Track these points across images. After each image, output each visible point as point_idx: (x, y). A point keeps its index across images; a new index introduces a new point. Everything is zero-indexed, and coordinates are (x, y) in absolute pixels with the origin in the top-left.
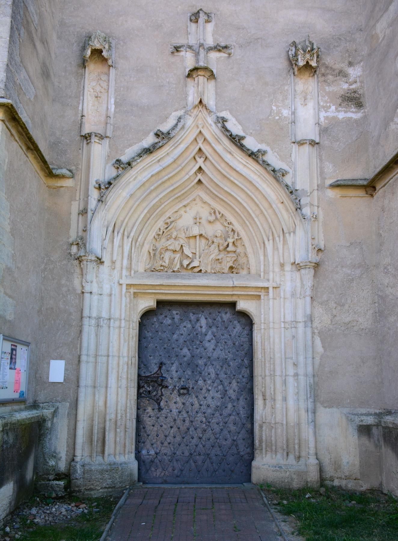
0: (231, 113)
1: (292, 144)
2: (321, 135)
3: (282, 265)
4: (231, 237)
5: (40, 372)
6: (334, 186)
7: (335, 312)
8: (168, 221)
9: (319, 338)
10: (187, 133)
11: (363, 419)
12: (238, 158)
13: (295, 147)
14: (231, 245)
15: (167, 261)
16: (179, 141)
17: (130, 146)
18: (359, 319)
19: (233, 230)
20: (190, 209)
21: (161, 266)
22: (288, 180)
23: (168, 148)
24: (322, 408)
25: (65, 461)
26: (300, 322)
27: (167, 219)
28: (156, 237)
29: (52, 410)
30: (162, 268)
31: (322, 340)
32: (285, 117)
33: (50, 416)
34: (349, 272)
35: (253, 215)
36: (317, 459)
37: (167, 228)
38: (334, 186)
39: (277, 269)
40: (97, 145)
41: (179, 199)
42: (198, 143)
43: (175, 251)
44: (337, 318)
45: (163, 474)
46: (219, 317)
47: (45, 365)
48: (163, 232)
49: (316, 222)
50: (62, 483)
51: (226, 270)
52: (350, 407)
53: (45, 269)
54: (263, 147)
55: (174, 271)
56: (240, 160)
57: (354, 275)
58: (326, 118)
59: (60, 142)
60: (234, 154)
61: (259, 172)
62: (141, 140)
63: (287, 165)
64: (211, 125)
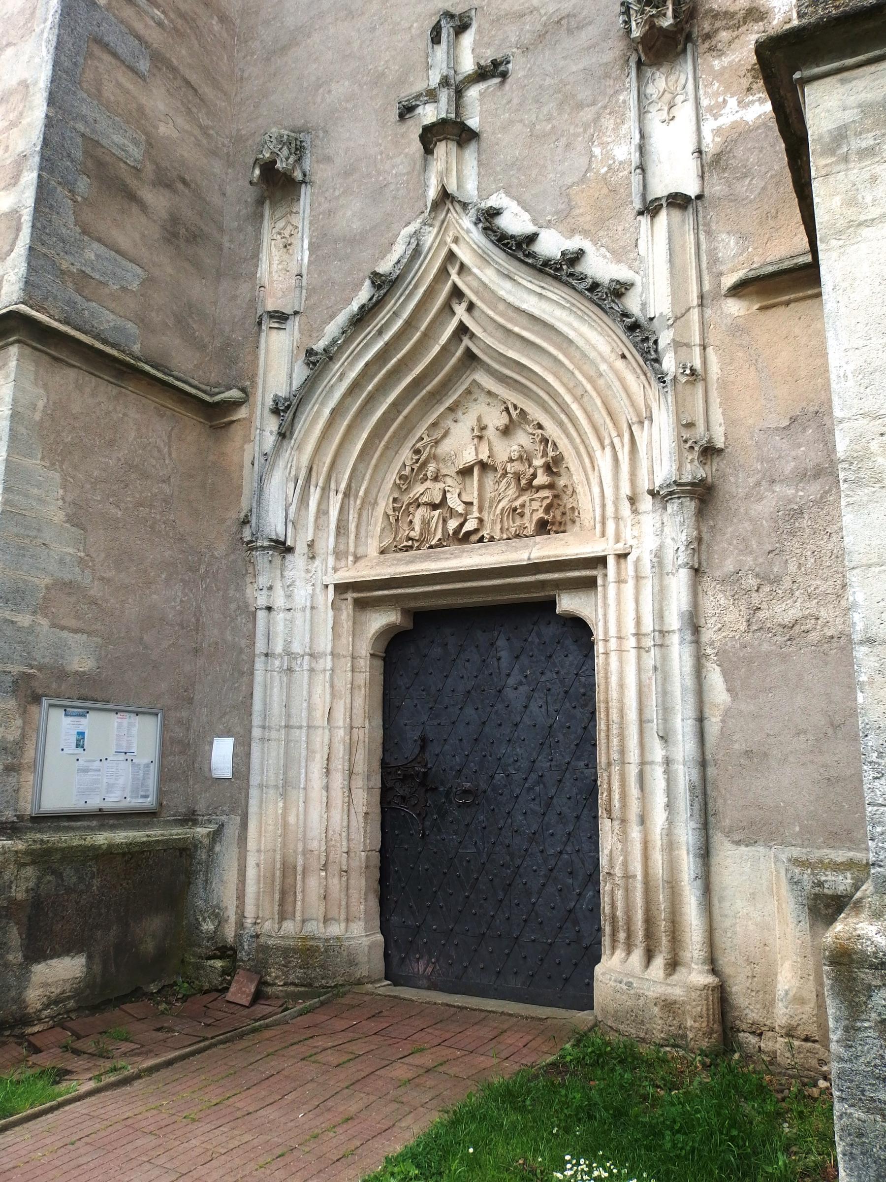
0: (508, 194)
1: (639, 218)
2: (707, 175)
5: (199, 759)
6: (739, 289)
7: (756, 599)
8: (419, 445)
9: (718, 669)
10: (427, 261)
11: (823, 878)
12: (524, 283)
14: (540, 472)
15: (417, 528)
16: (413, 283)
17: (332, 317)
18: (822, 609)
20: (464, 413)
22: (632, 303)
23: (393, 302)
24: (728, 845)
25: (234, 925)
26: (673, 631)
27: (417, 442)
28: (398, 482)
29: (213, 827)
31: (725, 673)
32: (620, 163)
33: (206, 841)
34: (791, 492)
35: (568, 399)
36: (714, 971)
38: (739, 289)
40: (274, 333)
41: (437, 396)
42: (449, 275)
44: (761, 615)
45: (429, 970)
46: (533, 634)
47: (207, 748)
48: (413, 469)
49: (700, 387)
50: (219, 964)
51: (531, 528)
52: (802, 846)
53: (207, 572)
54: (573, 244)
55: (431, 547)
56: (529, 285)
57: (801, 497)
58: (717, 132)
59: (228, 345)
60: (516, 277)
61: (568, 302)
62: (349, 301)
63: (630, 268)
64: (468, 232)
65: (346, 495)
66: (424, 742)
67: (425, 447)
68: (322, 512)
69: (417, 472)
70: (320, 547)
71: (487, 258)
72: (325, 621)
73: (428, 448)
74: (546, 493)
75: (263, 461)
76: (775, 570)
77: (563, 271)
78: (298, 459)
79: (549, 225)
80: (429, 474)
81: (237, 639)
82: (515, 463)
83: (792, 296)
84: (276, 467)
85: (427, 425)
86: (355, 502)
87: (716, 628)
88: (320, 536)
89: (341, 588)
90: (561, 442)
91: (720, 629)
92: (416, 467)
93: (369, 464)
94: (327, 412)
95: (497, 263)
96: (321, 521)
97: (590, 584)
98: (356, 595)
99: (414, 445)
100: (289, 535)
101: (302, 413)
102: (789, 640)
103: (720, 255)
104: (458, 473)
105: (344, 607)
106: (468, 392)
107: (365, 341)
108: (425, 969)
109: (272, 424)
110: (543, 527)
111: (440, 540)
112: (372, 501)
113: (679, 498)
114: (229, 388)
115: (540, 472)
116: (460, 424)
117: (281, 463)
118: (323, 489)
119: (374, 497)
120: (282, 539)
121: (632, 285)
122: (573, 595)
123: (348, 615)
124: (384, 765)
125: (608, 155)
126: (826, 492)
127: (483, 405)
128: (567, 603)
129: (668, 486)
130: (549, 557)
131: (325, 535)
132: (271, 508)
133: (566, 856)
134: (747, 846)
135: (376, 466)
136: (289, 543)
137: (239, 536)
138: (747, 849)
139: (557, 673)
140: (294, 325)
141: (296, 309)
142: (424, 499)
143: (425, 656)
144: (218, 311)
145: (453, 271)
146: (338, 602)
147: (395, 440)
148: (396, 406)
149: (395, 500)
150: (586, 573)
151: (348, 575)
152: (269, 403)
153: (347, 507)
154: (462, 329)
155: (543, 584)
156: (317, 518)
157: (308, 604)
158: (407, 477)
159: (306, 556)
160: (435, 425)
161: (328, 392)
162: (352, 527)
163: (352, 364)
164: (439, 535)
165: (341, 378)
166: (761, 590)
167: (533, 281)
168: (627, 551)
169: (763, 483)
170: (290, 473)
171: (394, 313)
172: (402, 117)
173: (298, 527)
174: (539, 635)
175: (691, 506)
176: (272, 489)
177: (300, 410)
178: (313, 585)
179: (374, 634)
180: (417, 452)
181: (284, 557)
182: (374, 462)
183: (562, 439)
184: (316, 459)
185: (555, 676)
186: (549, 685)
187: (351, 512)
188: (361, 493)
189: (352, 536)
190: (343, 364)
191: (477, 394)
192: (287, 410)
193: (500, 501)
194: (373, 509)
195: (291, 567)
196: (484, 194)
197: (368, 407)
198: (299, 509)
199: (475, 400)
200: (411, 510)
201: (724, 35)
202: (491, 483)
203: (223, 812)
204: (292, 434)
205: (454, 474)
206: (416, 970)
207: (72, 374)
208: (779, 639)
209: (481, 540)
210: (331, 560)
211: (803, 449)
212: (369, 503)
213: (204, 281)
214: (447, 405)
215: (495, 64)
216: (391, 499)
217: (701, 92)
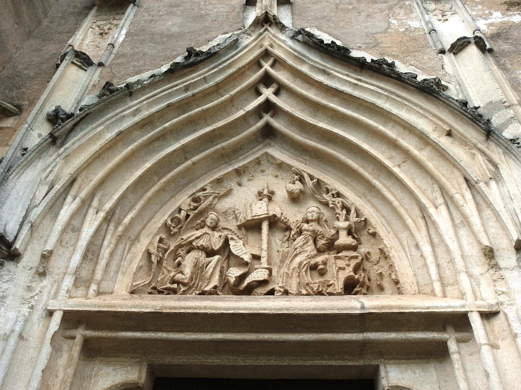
3: (489, 253)
4: (342, 218)
13: (447, 58)
16: (228, 62)
19: (344, 207)
20: (249, 180)
21: (173, 282)
23: (206, 69)
27: (198, 191)
30: (175, 286)
37: (196, 208)
39: (479, 267)
40: (74, 68)
43: (210, 253)
48: (188, 216)
51: (339, 286)
55: (203, 293)
61: (386, 90)
65: (107, 220)
67: (206, 197)
68: (72, 227)
69: (197, 216)
70: (57, 264)
72: (34, 362)
73: (211, 198)
75: (19, 154)
78: (62, 169)
80: (208, 222)
84: (32, 167)
85: (211, 179)
86: (116, 227)
88: (60, 253)
89: (72, 319)
90: (366, 210)
92: (192, 215)
93: (141, 197)
94: (110, 135)
95: (312, 61)
96: (67, 237)
97: (438, 353)
98: (90, 333)
99: (194, 194)
100: (22, 237)
101: (82, 130)
104: (240, 227)
105: (66, 347)
106: (258, 162)
107: (170, 91)
109: (44, 130)
110: (350, 287)
111: (215, 287)
112: (133, 237)
115: (343, 234)
116: (243, 189)
117: (40, 165)
118: (83, 202)
119: (136, 233)
120: (10, 238)
122: (414, 367)
123: (70, 358)
127: (271, 177)
130: (391, 307)
131: (67, 254)
132: (8, 202)
135: (150, 199)
136: (18, 245)
141: (103, 61)
142: (201, 242)
144: (17, 55)
146: (59, 339)
147: (173, 185)
148: (185, 152)
149: (161, 241)
151: (88, 302)
152: (50, 108)
153: (103, 232)
155: (363, 347)
156: (64, 231)
157: (18, 329)
158: (179, 220)
159: (33, 271)
160: (219, 181)
161: (117, 120)
162: (105, 253)
163: (150, 105)
164: (215, 281)
165: (135, 113)
167: (350, 74)
168: (494, 309)
170: (47, 177)
171: (204, 77)
173: (35, 235)
176: (18, 186)
177: (81, 125)
178: (32, 308)
180: (196, 200)
182: (149, 194)
183: (366, 208)
184: (84, 173)
187: (108, 237)
188: (126, 220)
189: (102, 263)
190: (141, 102)
191: (265, 165)
192: (63, 126)
193: (296, 255)
194: (131, 245)
195: (6, 278)
197: (157, 144)
198: (43, 216)
199: (263, 171)
200: (181, 252)
202: (279, 242)
204: (63, 144)
209: (272, 292)
210: (68, 282)
212: (129, 237)
213: (16, 26)
214: (236, 166)
216: (158, 238)
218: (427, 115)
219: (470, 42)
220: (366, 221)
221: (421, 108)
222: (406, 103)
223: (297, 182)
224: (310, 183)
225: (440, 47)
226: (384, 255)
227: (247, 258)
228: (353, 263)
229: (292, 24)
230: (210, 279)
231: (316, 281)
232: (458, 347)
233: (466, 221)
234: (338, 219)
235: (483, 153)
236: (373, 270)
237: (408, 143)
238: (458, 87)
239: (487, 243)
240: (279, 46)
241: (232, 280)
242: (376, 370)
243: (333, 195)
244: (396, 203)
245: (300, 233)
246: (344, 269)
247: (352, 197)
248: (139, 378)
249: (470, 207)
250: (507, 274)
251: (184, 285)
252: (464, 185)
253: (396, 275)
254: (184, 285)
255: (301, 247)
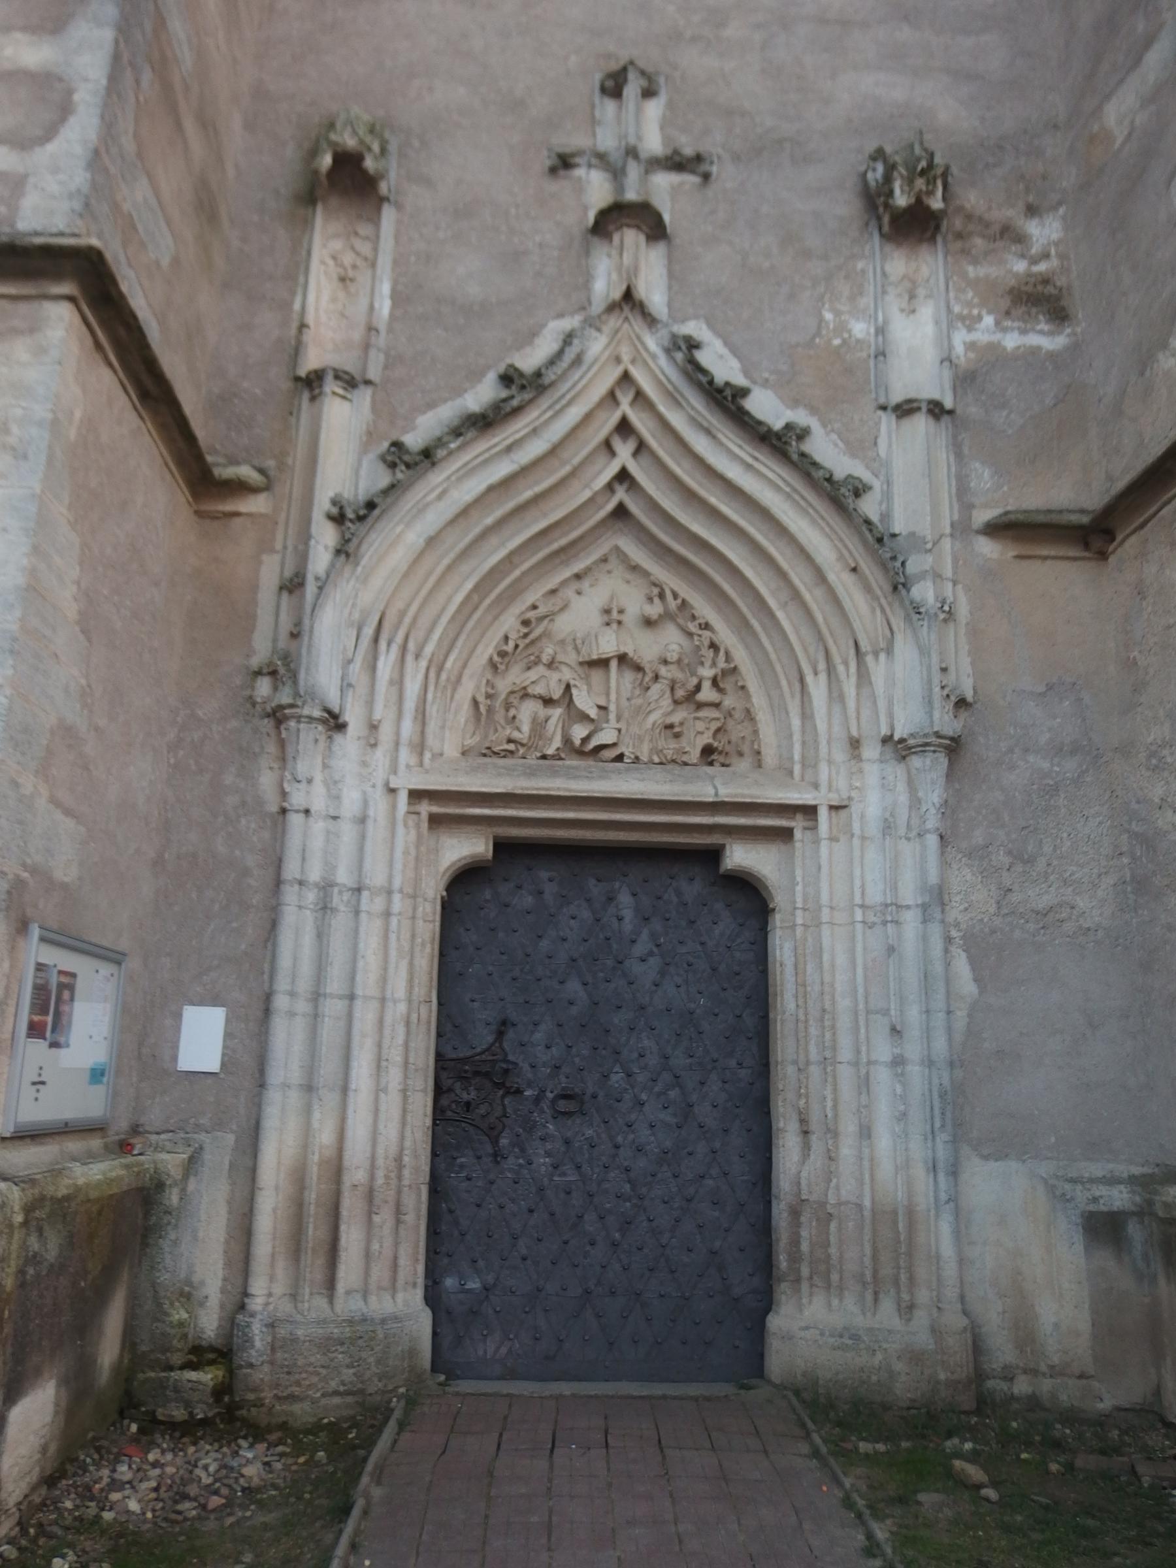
1: (880, 413)
3: (855, 744)
4: (708, 663)
6: (999, 529)
7: (1007, 880)
8: (531, 615)
9: (964, 955)
11: (1098, 1194)
13: (887, 421)
14: (707, 685)
15: (526, 728)
16: (568, 397)
17: (431, 406)
19: (713, 646)
20: (592, 586)
21: (510, 741)
22: (869, 507)
24: (976, 1161)
30: (511, 747)
31: (972, 961)
32: (858, 341)
34: (1046, 765)
37: (526, 635)
38: (999, 529)
40: (338, 400)
43: (548, 702)
44: (1015, 898)
45: (504, 1350)
47: (168, 1022)
48: (517, 646)
51: (695, 755)
55: (544, 757)
56: (737, 450)
57: (1058, 773)
60: (720, 436)
61: (788, 484)
62: (458, 392)
63: (867, 467)
66: (503, 1027)
71: (678, 397)
74: (714, 713)
76: (1030, 848)
77: (778, 443)
79: (765, 384)
80: (545, 658)
81: (237, 853)
82: (672, 667)
83: (1053, 553)
87: (962, 907)
89: (416, 795)
91: (966, 909)
92: (521, 646)
95: (693, 408)
97: (786, 835)
98: (436, 809)
99: (523, 613)
102: (1043, 928)
103: (972, 484)
106: (604, 560)
108: (498, 1348)
111: (558, 749)
113: (934, 752)
114: (237, 463)
115: (707, 685)
121: (870, 488)
122: (749, 846)
124: (439, 1057)
125: (841, 328)
126: (1083, 772)
128: (739, 856)
129: (925, 735)
130: (743, 796)
133: (710, 1182)
134: (996, 1160)
137: (248, 693)
138: (998, 1163)
139: (702, 944)
140: (364, 396)
143: (507, 906)
145: (625, 400)
150: (780, 824)
154: (623, 476)
160: (553, 592)
166: (1012, 870)
169: (1017, 750)
172: (553, 170)
174: (679, 893)
175: (943, 760)
179: (448, 869)
180: (526, 623)
181: (330, 737)
185: (699, 948)
186: (691, 959)
191: (614, 562)
192: (355, 519)
196: (677, 315)
199: (609, 572)
200: (514, 700)
201: (978, 242)
203: (198, 1128)
205: (573, 664)
206: (481, 1353)
207: (106, 375)
208: (1031, 926)
209: (620, 758)
211: (1059, 720)
215: (699, 158)
217: (952, 295)
218: (834, 537)
219: (919, 409)
220: (735, 668)
221: (828, 524)
222: (811, 511)
223: (656, 600)
224: (673, 604)
225: (882, 400)
226: (749, 716)
227: (593, 713)
228: (714, 726)
229: (670, 305)
230: (551, 740)
231: (670, 747)
232: (803, 834)
233: (842, 698)
234: (702, 663)
235: (883, 611)
236: (737, 731)
237: (799, 577)
238: (885, 487)
239: (855, 733)
240: (645, 363)
241: (577, 742)
242: (723, 846)
243: (700, 625)
244: (773, 656)
245: (656, 677)
246: (702, 733)
247: (725, 634)
248: (487, 850)
249: (850, 688)
250: (866, 767)
251: (523, 745)
252: (852, 652)
253: (759, 746)
254: (523, 745)
255: (657, 701)
